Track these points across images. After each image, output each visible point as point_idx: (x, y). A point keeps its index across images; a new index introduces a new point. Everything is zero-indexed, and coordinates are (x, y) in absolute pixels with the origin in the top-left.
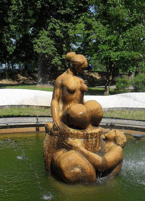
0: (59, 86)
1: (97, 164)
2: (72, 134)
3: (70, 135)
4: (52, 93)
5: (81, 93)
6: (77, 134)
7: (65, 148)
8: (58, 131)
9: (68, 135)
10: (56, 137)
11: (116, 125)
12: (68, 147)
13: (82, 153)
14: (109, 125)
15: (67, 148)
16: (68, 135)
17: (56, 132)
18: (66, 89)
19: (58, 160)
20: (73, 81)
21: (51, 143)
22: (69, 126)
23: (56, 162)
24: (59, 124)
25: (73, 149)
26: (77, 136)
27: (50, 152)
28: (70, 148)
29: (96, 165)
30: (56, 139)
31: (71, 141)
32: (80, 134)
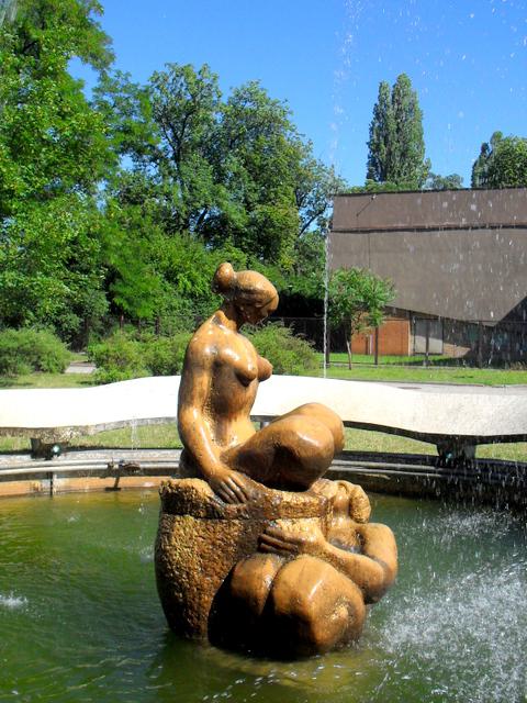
0: (208, 364)
1: (375, 583)
2: (288, 506)
3: (283, 512)
4: (176, 380)
5: (196, 375)
6: (304, 504)
7: (274, 552)
8: (241, 502)
9: (276, 512)
10: (237, 522)
11: (141, 466)
12: (283, 548)
13: (332, 559)
14: (116, 466)
15: (284, 552)
16: (276, 512)
17: (234, 506)
18: (233, 375)
19: (280, 593)
20: (223, 339)
21: (213, 544)
22: (271, 485)
23: (270, 597)
24: (132, 489)
25: (303, 553)
26: (302, 512)
27: (211, 572)
28: (291, 549)
29: (372, 586)
30: (236, 528)
31: (285, 526)
32: (312, 505)
